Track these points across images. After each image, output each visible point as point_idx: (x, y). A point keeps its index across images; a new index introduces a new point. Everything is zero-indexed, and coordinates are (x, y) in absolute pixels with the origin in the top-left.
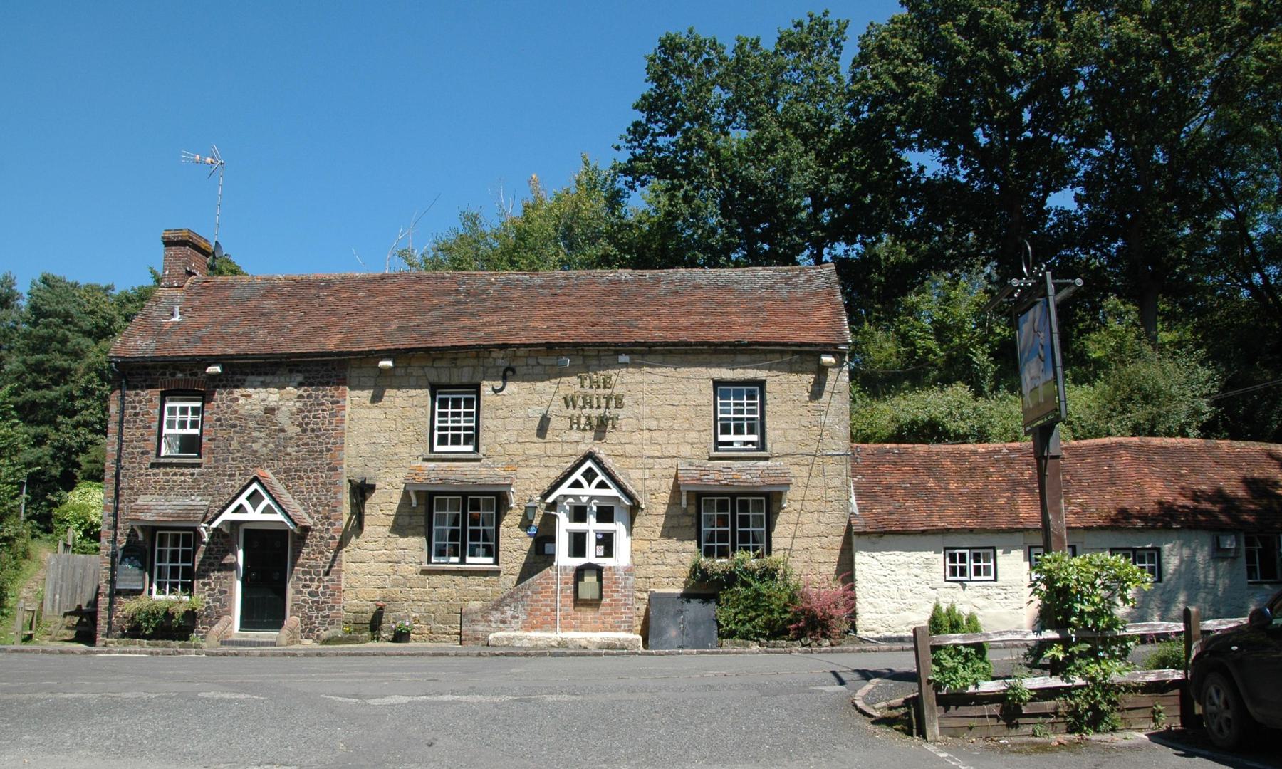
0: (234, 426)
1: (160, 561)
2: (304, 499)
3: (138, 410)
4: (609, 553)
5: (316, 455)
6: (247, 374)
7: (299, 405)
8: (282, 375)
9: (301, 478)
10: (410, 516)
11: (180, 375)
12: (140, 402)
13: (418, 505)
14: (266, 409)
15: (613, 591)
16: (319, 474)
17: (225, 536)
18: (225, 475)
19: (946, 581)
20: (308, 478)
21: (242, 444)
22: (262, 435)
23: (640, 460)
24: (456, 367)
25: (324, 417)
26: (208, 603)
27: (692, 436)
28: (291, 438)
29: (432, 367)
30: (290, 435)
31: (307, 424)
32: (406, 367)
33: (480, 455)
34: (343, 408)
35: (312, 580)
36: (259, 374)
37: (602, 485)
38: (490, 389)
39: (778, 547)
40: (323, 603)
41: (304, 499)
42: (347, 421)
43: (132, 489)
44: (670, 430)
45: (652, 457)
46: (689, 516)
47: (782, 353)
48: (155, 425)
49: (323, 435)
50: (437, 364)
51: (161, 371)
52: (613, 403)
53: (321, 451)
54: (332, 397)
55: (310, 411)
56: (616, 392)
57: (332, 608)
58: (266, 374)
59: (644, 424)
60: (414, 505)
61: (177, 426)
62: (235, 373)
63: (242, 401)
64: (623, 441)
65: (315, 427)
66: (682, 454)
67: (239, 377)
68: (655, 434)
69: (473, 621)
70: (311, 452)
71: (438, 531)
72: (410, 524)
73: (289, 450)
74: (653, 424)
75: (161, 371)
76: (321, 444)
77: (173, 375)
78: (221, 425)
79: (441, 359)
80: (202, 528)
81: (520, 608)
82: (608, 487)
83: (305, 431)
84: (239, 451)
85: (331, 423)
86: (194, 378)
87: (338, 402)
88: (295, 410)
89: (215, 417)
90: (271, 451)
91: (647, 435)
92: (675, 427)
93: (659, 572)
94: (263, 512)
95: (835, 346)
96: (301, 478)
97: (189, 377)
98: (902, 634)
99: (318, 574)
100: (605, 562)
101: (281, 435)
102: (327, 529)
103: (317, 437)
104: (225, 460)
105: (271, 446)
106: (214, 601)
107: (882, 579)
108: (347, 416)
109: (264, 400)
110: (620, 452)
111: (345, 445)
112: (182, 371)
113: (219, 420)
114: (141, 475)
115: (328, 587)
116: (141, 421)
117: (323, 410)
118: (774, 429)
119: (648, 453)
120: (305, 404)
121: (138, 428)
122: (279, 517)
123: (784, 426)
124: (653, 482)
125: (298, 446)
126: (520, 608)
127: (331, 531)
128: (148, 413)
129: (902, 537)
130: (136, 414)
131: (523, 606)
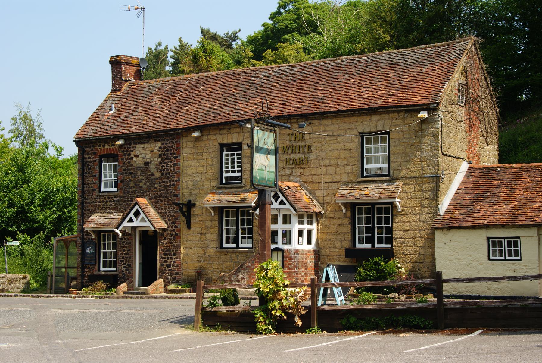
0: (131, 173)
1: (104, 249)
2: (163, 213)
3: (90, 167)
4: (289, 242)
5: (168, 188)
6: (136, 144)
7: (159, 160)
8: (151, 143)
9: (161, 201)
10: (212, 221)
11: (107, 146)
12: (91, 162)
13: (215, 214)
14: (145, 163)
15: (289, 264)
16: (169, 199)
17: (129, 234)
18: (128, 201)
19: (489, 259)
20: (165, 201)
21: (135, 183)
22: (144, 178)
23: (321, 185)
24: (230, 133)
25: (171, 166)
26: (123, 271)
27: (348, 168)
28: (157, 179)
29: (219, 134)
30: (155, 177)
31: (164, 170)
32: (208, 135)
33: (242, 185)
34: (179, 161)
35: (168, 258)
36: (142, 143)
37: (282, 203)
38: (246, 145)
39: (396, 237)
40: (173, 270)
41: (163, 213)
42: (181, 168)
43: (89, 210)
44: (337, 165)
45: (328, 183)
46: (347, 218)
47: (399, 112)
48: (97, 175)
49: (171, 176)
50: (222, 132)
51: (99, 144)
52: (306, 149)
53: (170, 185)
54: (174, 154)
55: (164, 163)
56: (307, 144)
57: (177, 274)
58: (145, 143)
59: (323, 162)
60: (213, 215)
61: (373, 151)
62: (131, 144)
63: (134, 159)
64: (312, 173)
65: (167, 172)
66: (343, 180)
67: (133, 145)
68: (329, 168)
69: (225, 281)
70: (166, 186)
71: (242, 229)
72: (211, 226)
73: (156, 186)
74: (327, 162)
75: (99, 144)
76: (170, 181)
77: (104, 146)
78: (126, 173)
79: (223, 129)
80: (117, 231)
81: (246, 274)
82: (285, 204)
83: (162, 174)
84: (134, 187)
85: (174, 169)
86: (114, 147)
87: (177, 157)
88: (158, 163)
89: (123, 168)
90: (148, 186)
91: (324, 169)
92: (339, 164)
93: (332, 252)
94: (140, 222)
95: (428, 105)
96: (161, 201)
97: (111, 147)
98: (463, 294)
99: (170, 254)
100: (286, 247)
101: (152, 177)
102: (174, 230)
103: (168, 177)
104: (128, 192)
105: (148, 184)
106: (126, 270)
107: (450, 257)
108: (181, 165)
109: (144, 158)
110: (311, 180)
111: (181, 182)
112: (108, 144)
113: (125, 170)
114: (92, 202)
115: (175, 263)
116: (92, 173)
117: (171, 162)
118: (394, 162)
119: (326, 180)
120: (162, 160)
121: (90, 177)
122: (148, 224)
123: (400, 159)
124: (328, 198)
125: (160, 183)
126: (246, 274)
127: (176, 230)
128: (94, 168)
129: (461, 230)
130: (89, 169)
131: (247, 272)
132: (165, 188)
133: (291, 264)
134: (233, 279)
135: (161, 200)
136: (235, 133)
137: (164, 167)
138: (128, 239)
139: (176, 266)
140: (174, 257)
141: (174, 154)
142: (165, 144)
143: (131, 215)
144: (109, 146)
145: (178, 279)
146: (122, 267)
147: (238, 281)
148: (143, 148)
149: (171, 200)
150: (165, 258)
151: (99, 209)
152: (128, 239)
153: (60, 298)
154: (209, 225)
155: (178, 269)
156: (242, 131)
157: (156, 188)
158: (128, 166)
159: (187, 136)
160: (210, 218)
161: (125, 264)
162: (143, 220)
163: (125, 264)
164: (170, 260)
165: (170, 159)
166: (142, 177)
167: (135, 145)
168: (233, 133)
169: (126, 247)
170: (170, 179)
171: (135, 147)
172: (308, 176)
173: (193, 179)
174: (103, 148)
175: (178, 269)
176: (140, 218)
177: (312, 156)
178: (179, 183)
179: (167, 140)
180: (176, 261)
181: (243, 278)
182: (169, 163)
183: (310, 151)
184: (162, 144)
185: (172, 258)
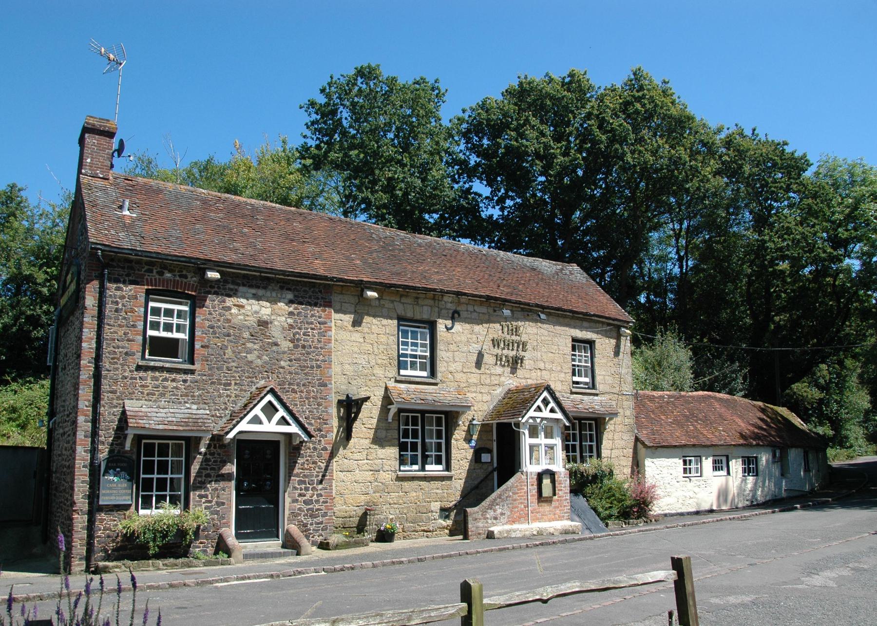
6: (239, 285)
8: (274, 290)
10: (387, 430)
12: (123, 297)
14: (259, 321)
20: (302, 392)
29: (400, 302)
35: (307, 489)
38: (444, 327)
56: (523, 339)
58: (258, 287)
63: (234, 310)
72: (386, 437)
73: (283, 363)
76: (311, 360)
81: (506, 507)
83: (296, 347)
86: (185, 280)
87: (325, 323)
97: (178, 278)
101: (275, 348)
103: (308, 353)
115: (321, 496)
123: (604, 373)
125: (290, 360)
126: (506, 507)
128: (132, 311)
132: (302, 370)
133: (561, 490)
134: (488, 516)
135: (293, 389)
136: (426, 305)
137: (299, 334)
138: (219, 454)
139: (323, 502)
140: (320, 487)
141: (320, 317)
142: (302, 297)
143: (257, 411)
144: (175, 276)
145: (326, 523)
146: (203, 506)
147: (496, 518)
148: (253, 294)
149: (313, 391)
150: (301, 489)
151: (142, 393)
152: (219, 454)
153: (493, 548)
154: (383, 436)
155: (325, 506)
156: (437, 305)
157: (283, 368)
158: (219, 320)
159: (342, 294)
160: (383, 425)
161: (210, 502)
162: (283, 421)
163: (210, 502)
164: (311, 492)
165: (312, 323)
166: (252, 345)
167: (236, 287)
168: (423, 306)
169: (212, 469)
170: (311, 357)
171: (236, 290)
172: (521, 379)
173: (355, 362)
174: (157, 277)
175: (325, 506)
176: (277, 417)
177: (527, 355)
178: (330, 365)
179: (305, 291)
180: (323, 494)
181: (502, 514)
182: (309, 330)
183: (524, 350)
184: (295, 296)
185: (314, 489)
